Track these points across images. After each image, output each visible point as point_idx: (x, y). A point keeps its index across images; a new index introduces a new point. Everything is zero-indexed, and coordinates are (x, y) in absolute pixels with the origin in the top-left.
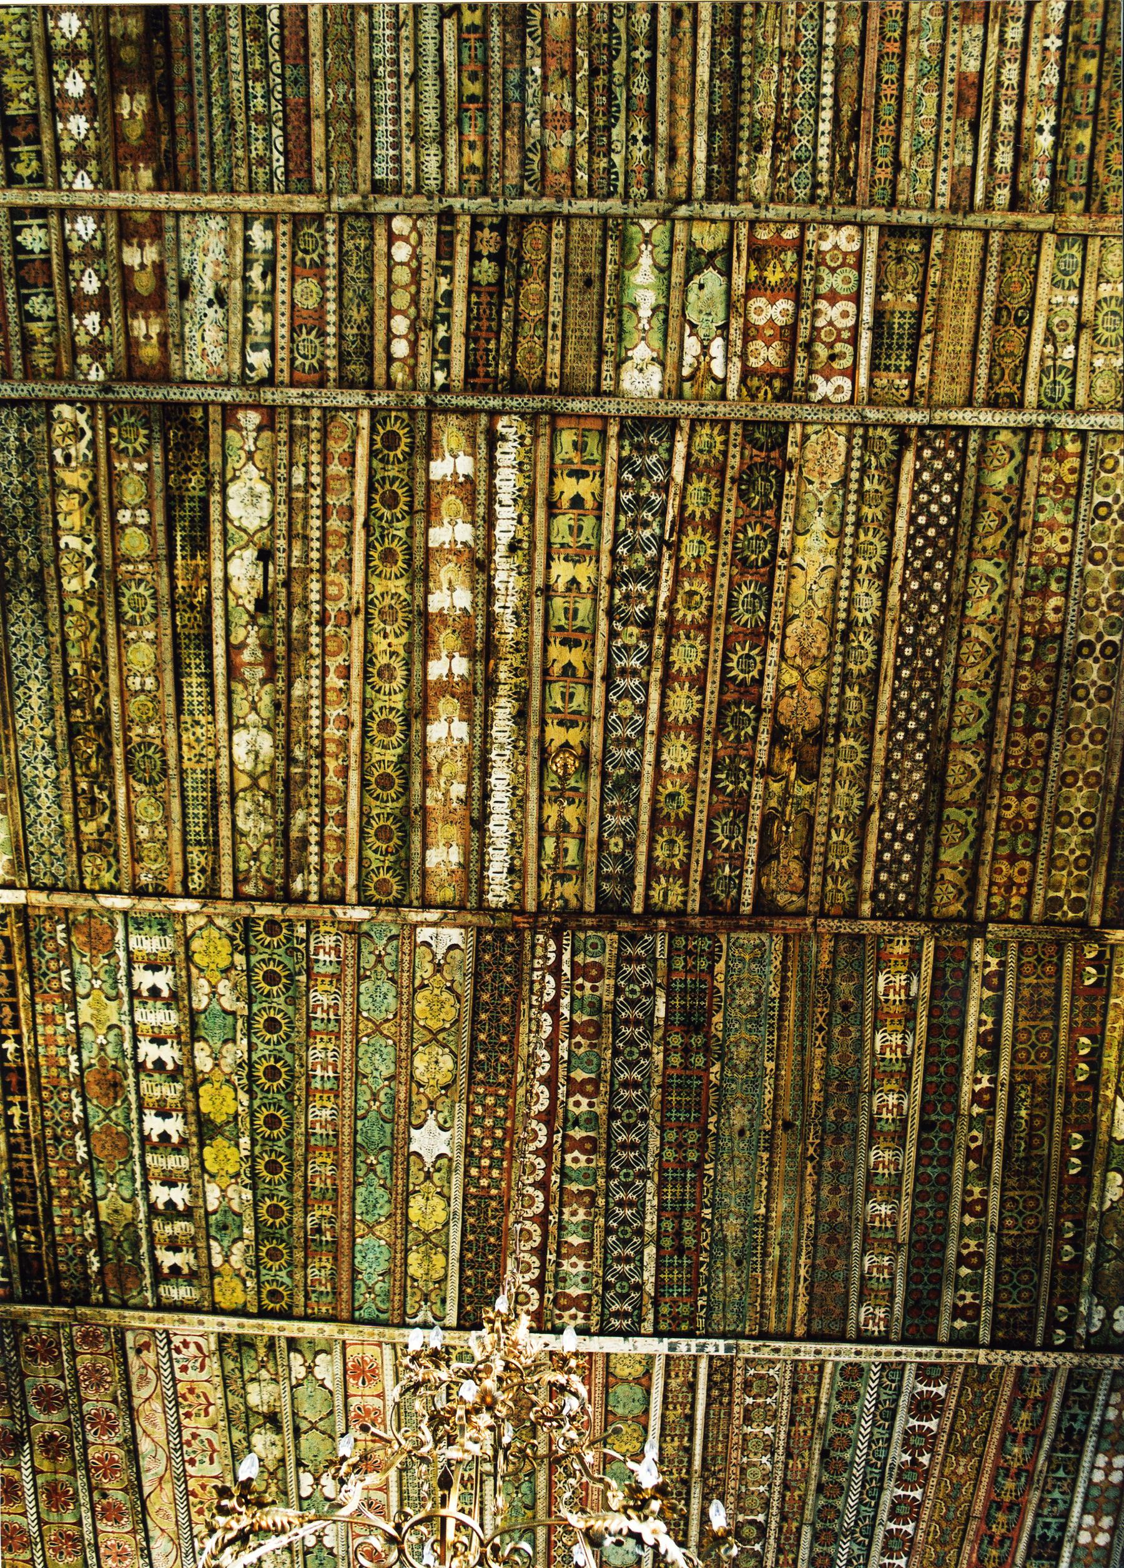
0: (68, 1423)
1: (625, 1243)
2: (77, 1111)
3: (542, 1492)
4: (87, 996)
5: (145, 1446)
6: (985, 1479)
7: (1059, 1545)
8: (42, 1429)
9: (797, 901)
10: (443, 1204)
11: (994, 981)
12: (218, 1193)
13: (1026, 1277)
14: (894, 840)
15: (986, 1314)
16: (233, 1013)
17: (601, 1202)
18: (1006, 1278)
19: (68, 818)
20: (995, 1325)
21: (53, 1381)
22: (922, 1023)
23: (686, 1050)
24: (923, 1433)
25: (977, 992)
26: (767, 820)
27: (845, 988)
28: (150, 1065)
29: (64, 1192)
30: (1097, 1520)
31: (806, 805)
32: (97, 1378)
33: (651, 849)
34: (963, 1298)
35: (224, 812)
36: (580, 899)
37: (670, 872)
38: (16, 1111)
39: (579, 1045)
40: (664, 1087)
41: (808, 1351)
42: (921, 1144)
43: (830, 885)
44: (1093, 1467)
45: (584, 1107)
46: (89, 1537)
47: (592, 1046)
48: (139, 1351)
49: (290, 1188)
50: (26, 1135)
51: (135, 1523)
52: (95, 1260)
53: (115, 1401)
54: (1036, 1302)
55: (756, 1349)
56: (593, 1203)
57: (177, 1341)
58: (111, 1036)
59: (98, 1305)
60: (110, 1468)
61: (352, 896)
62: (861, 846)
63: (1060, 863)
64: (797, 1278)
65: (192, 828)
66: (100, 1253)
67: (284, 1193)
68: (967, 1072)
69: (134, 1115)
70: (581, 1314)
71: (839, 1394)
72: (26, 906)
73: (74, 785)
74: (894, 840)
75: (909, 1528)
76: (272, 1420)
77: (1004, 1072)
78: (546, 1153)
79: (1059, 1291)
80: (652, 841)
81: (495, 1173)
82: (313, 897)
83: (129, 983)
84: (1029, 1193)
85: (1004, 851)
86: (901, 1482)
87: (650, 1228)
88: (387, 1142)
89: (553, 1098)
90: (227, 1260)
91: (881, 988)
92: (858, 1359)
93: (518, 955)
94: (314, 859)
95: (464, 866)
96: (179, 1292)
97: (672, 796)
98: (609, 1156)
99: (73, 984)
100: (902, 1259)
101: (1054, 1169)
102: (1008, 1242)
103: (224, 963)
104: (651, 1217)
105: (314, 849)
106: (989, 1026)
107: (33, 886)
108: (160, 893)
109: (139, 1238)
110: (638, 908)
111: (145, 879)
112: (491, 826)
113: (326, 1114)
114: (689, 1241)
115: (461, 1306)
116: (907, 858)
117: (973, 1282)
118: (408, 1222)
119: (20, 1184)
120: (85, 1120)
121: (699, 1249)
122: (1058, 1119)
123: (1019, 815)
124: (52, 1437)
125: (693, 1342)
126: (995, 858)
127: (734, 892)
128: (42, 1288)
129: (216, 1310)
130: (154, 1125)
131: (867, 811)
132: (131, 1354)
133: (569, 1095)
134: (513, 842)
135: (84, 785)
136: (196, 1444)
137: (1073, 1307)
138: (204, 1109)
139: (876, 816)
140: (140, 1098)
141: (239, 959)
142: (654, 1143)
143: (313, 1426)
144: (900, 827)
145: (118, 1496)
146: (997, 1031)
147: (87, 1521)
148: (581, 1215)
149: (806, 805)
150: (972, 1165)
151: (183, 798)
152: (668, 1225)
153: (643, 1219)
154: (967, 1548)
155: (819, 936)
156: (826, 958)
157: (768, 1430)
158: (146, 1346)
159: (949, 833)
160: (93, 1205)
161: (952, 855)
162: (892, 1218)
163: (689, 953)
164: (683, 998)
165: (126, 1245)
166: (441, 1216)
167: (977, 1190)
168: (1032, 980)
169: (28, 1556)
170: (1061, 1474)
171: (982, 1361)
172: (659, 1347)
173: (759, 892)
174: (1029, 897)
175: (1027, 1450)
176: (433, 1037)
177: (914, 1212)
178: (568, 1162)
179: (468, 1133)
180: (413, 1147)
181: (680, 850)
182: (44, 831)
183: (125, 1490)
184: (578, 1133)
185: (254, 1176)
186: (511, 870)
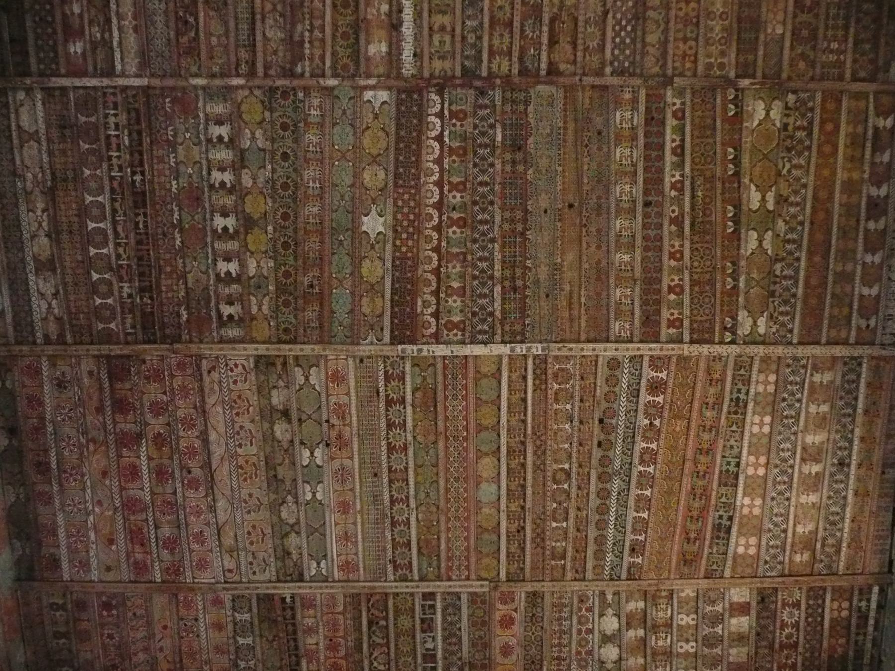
0: (168, 424)
1: (483, 284)
2: (176, 216)
3: (441, 454)
4: (182, 144)
5: (213, 436)
6: (692, 433)
7: (737, 477)
8: (153, 430)
9: (571, 68)
10: (381, 264)
11: (679, 115)
12: (255, 265)
13: (707, 300)
14: (621, 30)
15: (686, 323)
16: (264, 150)
17: (469, 258)
18: (696, 300)
19: (172, 33)
20: (692, 330)
21: (159, 396)
22: (642, 141)
23: (514, 162)
24: (654, 405)
25: (671, 122)
26: (553, 21)
27: (598, 121)
28: (217, 185)
29: (168, 269)
30: (757, 459)
31: (573, 11)
32: (185, 391)
33: (490, 40)
34: (672, 314)
35: (258, 24)
36: (453, 70)
37: (501, 53)
38: (141, 219)
39: (454, 161)
40: (503, 185)
41: (588, 349)
42: (646, 215)
43: (588, 57)
44: (752, 424)
45: (459, 198)
46: (180, 500)
47: (462, 161)
48: (209, 372)
49: (296, 259)
50: (147, 234)
51: (207, 490)
52: (185, 313)
53: (195, 407)
54: (714, 315)
55: (559, 349)
56: (465, 260)
57: (231, 364)
58: (196, 169)
59: (186, 342)
60: (192, 452)
61: (328, 72)
62: (604, 35)
63: (711, 41)
64: (580, 304)
65: (242, 38)
66: (188, 308)
67: (292, 263)
68: (667, 170)
69: (208, 216)
70: (460, 333)
71: (607, 380)
72: (148, 87)
73: (176, 13)
74: (621, 30)
75: (651, 469)
76: (286, 413)
77: (687, 169)
78: (438, 228)
79: (726, 308)
80: (491, 35)
81: (410, 243)
82: (307, 74)
83: (206, 134)
84: (705, 245)
85: (680, 35)
86: (646, 439)
87: (497, 274)
88: (350, 226)
89: (441, 193)
90: (260, 309)
91: (618, 121)
92: (616, 353)
93: (420, 106)
94: (307, 51)
95: (389, 53)
96: (233, 332)
97: (500, 8)
98: (474, 228)
99: (174, 136)
100: (638, 289)
101: (719, 229)
102: (695, 277)
103: (258, 118)
104: (497, 267)
105: (307, 45)
106: (678, 143)
107: (152, 75)
108: (223, 75)
109: (210, 296)
110: (484, 73)
111: (216, 69)
112: (404, 30)
113: (315, 209)
114: (519, 283)
115: (392, 332)
116: (628, 41)
117: (678, 304)
118: (362, 278)
119: (142, 266)
120: (180, 221)
121: (525, 287)
122: (719, 197)
123: (687, 14)
124: (159, 434)
125: (524, 346)
126: (675, 40)
127: (536, 64)
128: (154, 334)
129: (253, 341)
130: (220, 222)
131: (606, 13)
132: (205, 374)
133: (450, 191)
134: (415, 38)
135: (181, 14)
136: (242, 433)
137: (734, 318)
138: (248, 211)
139: (610, 16)
140: (212, 206)
141: (267, 114)
142: (498, 219)
143: (310, 417)
144: (623, 23)
145: (197, 472)
146: (682, 146)
147: (179, 491)
148: (459, 269)
149: (573, 11)
150: (673, 228)
151: (236, 18)
152: (508, 273)
153: (493, 270)
154: (685, 480)
155: (583, 88)
156: (587, 101)
157: (568, 406)
158: (214, 368)
159: (651, 26)
160: (184, 276)
161: (652, 38)
162: (631, 264)
163: (513, 102)
164: (511, 129)
165: (202, 303)
166: (380, 272)
167: (677, 244)
168: (699, 113)
169: (144, 517)
170: (734, 428)
171: (686, 353)
172: (505, 350)
173: (551, 63)
174: (695, 61)
175: (715, 413)
176: (375, 160)
177: (643, 259)
178: (451, 234)
179: (395, 218)
180: (364, 228)
181: (506, 40)
182: (159, 43)
183: (201, 467)
184: (456, 215)
185: (275, 251)
186: (415, 55)
